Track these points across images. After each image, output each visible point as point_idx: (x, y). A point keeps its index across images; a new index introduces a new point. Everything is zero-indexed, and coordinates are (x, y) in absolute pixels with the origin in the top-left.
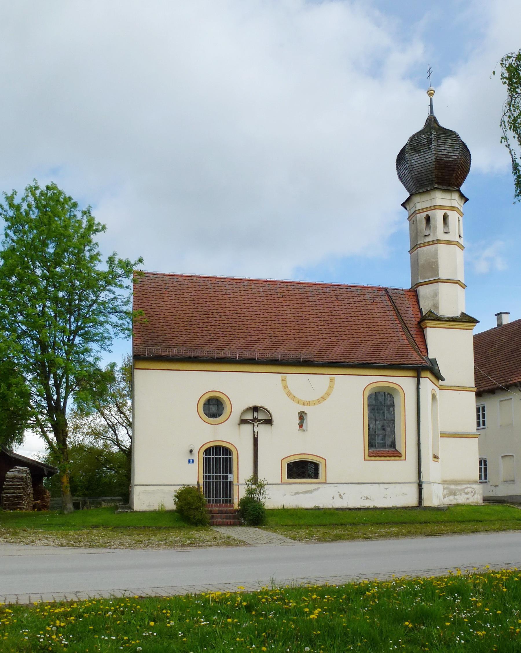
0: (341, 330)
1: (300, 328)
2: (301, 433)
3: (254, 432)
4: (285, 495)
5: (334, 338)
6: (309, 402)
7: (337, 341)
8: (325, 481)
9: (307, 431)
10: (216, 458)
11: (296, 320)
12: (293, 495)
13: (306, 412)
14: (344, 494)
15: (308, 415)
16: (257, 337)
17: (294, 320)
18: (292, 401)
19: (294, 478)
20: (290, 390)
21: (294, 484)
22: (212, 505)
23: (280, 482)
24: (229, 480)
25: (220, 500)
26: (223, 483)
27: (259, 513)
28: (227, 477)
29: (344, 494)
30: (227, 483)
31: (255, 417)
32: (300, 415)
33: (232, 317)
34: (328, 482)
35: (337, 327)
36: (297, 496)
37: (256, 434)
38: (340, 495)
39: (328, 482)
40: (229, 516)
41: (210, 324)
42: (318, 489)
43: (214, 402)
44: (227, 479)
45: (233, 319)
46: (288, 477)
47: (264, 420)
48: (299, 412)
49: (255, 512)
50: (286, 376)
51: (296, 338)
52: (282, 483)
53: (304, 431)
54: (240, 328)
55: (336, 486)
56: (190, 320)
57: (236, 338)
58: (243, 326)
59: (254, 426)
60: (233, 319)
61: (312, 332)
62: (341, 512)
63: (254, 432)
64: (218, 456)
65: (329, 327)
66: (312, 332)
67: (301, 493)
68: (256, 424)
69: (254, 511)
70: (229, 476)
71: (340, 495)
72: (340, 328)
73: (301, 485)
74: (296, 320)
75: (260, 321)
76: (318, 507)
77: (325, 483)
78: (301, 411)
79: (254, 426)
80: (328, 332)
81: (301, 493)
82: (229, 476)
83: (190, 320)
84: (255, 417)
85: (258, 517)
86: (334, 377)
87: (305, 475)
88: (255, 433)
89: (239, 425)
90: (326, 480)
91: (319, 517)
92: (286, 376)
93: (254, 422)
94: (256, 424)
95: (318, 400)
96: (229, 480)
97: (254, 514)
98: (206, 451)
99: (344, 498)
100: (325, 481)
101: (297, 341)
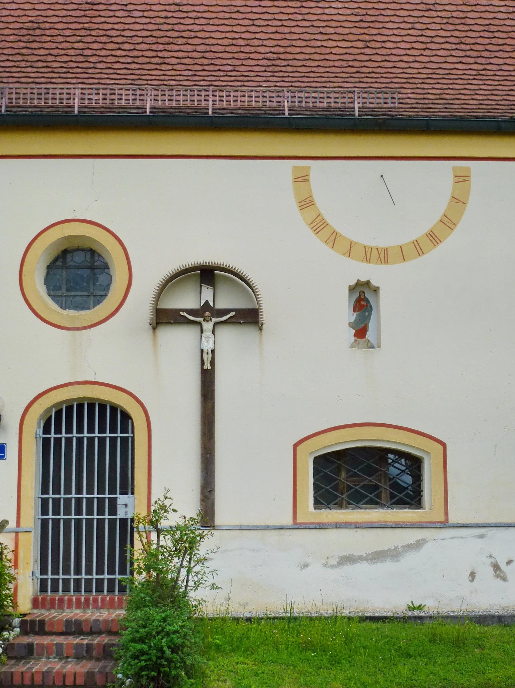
0: (494, 41)
1: (368, 38)
2: (360, 353)
3: (202, 351)
4: (306, 566)
5: (472, 60)
6: (386, 250)
7: (481, 67)
8: (442, 519)
9: (379, 346)
10: (113, 441)
11: (358, 18)
12: (332, 567)
13: (374, 283)
14: (509, 562)
15: (382, 293)
16: (230, 62)
17: (349, 18)
18: (326, 249)
19: (340, 506)
20: (323, 212)
21: (337, 526)
22: (61, 601)
23: (288, 520)
24: (121, 514)
25: (89, 582)
26: (100, 522)
27: (161, 650)
28: (113, 503)
29: (509, 562)
30: (112, 522)
31: (207, 302)
32: (356, 295)
33: (164, 14)
34: (452, 519)
35: (482, 34)
36: (348, 568)
37: (207, 358)
38: (496, 567)
39: (452, 519)
40: (89, 647)
41: (93, 33)
42: (419, 545)
43: (79, 258)
44: (113, 510)
45: (167, 18)
46: (318, 503)
47: (237, 311)
48: (353, 283)
49: (145, 647)
50: (309, 168)
51: (351, 63)
52: (297, 526)
53: (372, 347)
54: (181, 41)
55: (481, 537)
56: (35, 25)
57: (164, 67)
58: (193, 34)
59: (202, 332)
60: (167, 18)
61: (403, 45)
62: (495, 630)
63: (202, 351)
64: (119, 435)
65: (457, 34)
66: (403, 45)
67: (361, 559)
68: (208, 326)
69: (142, 640)
70: (122, 499)
71: (496, 567)
72: (491, 35)
73: (360, 532)
74: (358, 18)
75: (246, 22)
76: (420, 608)
77: (444, 525)
78: (368, 283)
79: (202, 332)
80: (454, 47)
81: (361, 559)
82: (122, 499)
83: (35, 25)
84: (207, 302)
85: (157, 667)
86: (468, 169)
87: (379, 496)
88: (205, 356)
89: (154, 329)
90: (446, 514)
91: (409, 656)
92: (309, 168)
93: (200, 320)
94: (208, 326)
95: (416, 243)
96: (121, 514)
97: (143, 653)
98: (126, 417)
99: (509, 576)
100: (442, 519)
101: (354, 70)
